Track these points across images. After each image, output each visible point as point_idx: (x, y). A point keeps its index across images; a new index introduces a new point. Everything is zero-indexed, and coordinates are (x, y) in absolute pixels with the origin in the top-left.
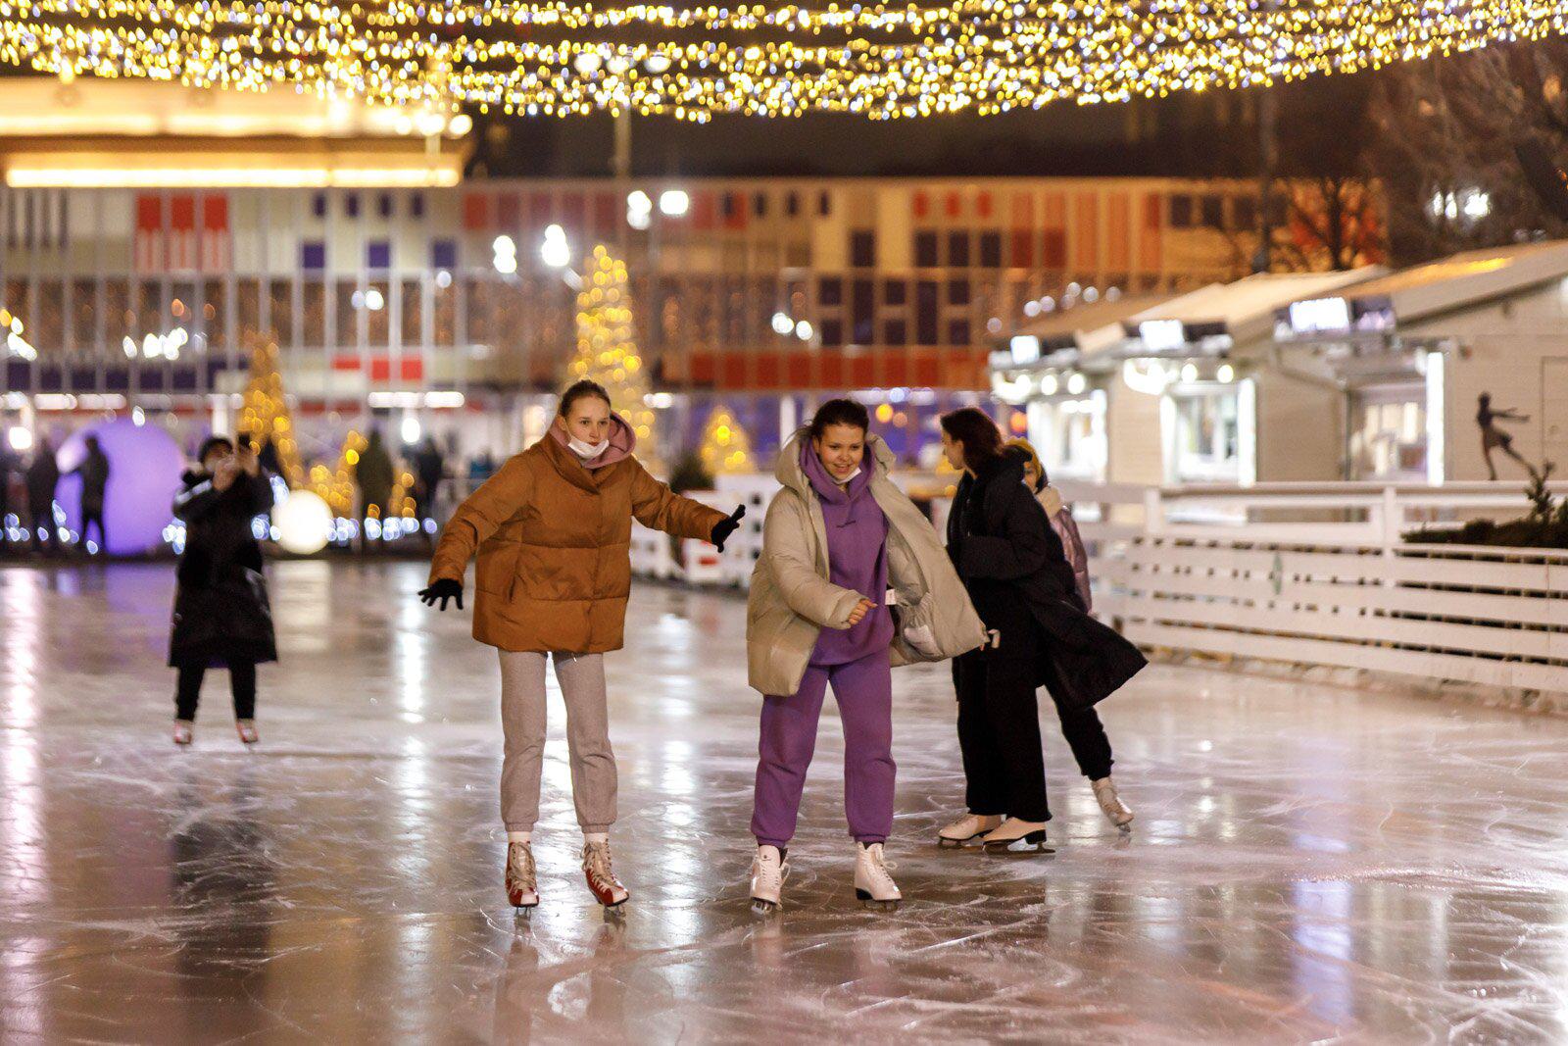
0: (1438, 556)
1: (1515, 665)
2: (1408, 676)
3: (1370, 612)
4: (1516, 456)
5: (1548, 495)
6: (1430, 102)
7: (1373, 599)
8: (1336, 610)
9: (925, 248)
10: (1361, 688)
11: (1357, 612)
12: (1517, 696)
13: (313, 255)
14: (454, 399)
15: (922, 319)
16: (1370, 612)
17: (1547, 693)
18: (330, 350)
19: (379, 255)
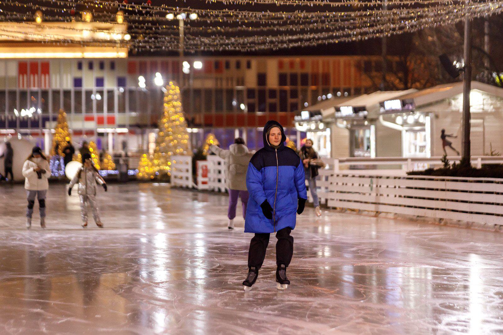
0: (416, 179)
1: (437, 211)
2: (408, 215)
3: (397, 196)
4: (453, 149)
5: (448, 161)
6: (431, 37)
7: (398, 192)
8: (388, 196)
9: (282, 79)
10: (395, 219)
11: (394, 196)
12: (438, 220)
13: (78, 82)
14: (125, 130)
15: (280, 104)
16: (397, 196)
17: (446, 219)
18: (84, 114)
19: (100, 82)
